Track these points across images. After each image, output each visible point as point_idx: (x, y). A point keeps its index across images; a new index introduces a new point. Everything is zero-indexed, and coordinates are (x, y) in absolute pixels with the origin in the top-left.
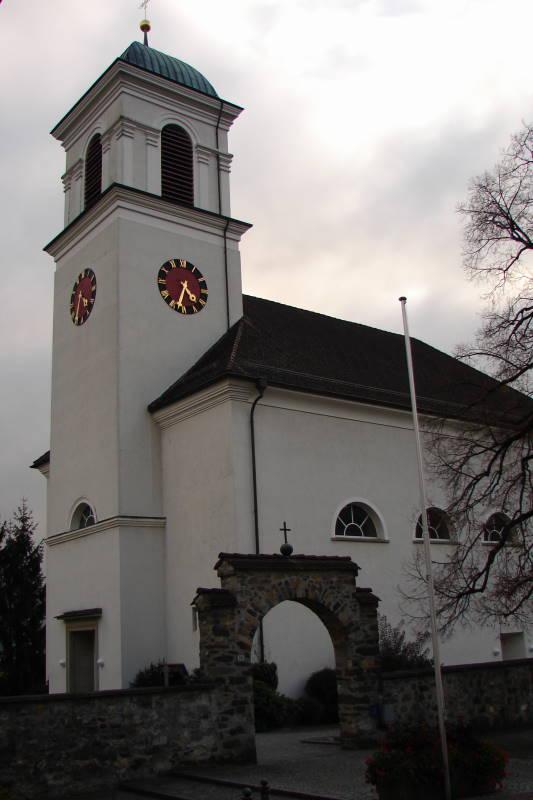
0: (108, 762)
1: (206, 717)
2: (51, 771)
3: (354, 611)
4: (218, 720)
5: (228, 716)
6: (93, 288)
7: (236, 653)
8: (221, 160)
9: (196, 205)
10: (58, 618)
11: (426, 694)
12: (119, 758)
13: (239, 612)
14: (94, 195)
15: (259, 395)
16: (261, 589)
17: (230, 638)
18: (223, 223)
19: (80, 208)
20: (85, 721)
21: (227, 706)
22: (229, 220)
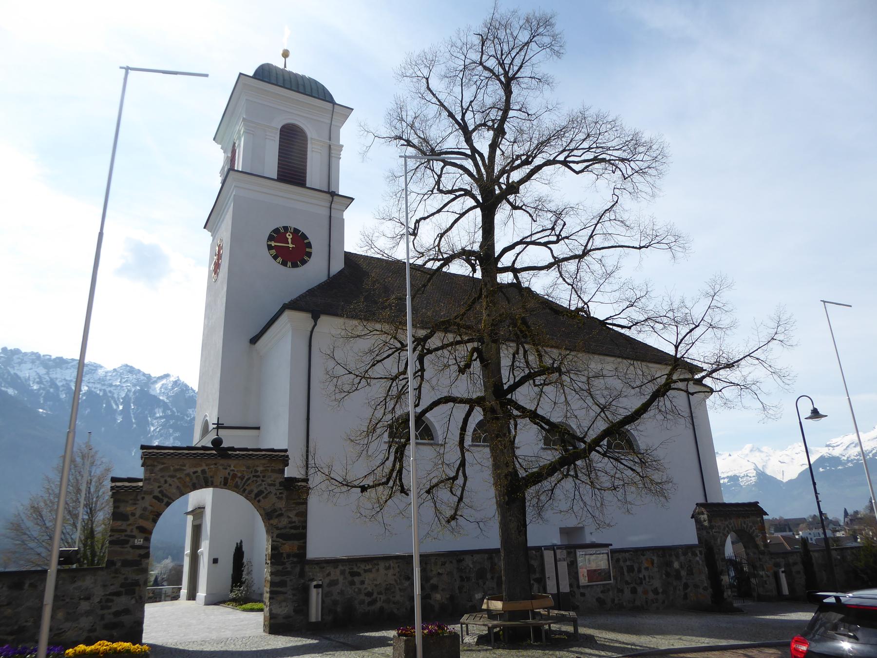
1: (87, 598)
4: (100, 602)
5: (114, 598)
13: (143, 498)
16: (172, 477)
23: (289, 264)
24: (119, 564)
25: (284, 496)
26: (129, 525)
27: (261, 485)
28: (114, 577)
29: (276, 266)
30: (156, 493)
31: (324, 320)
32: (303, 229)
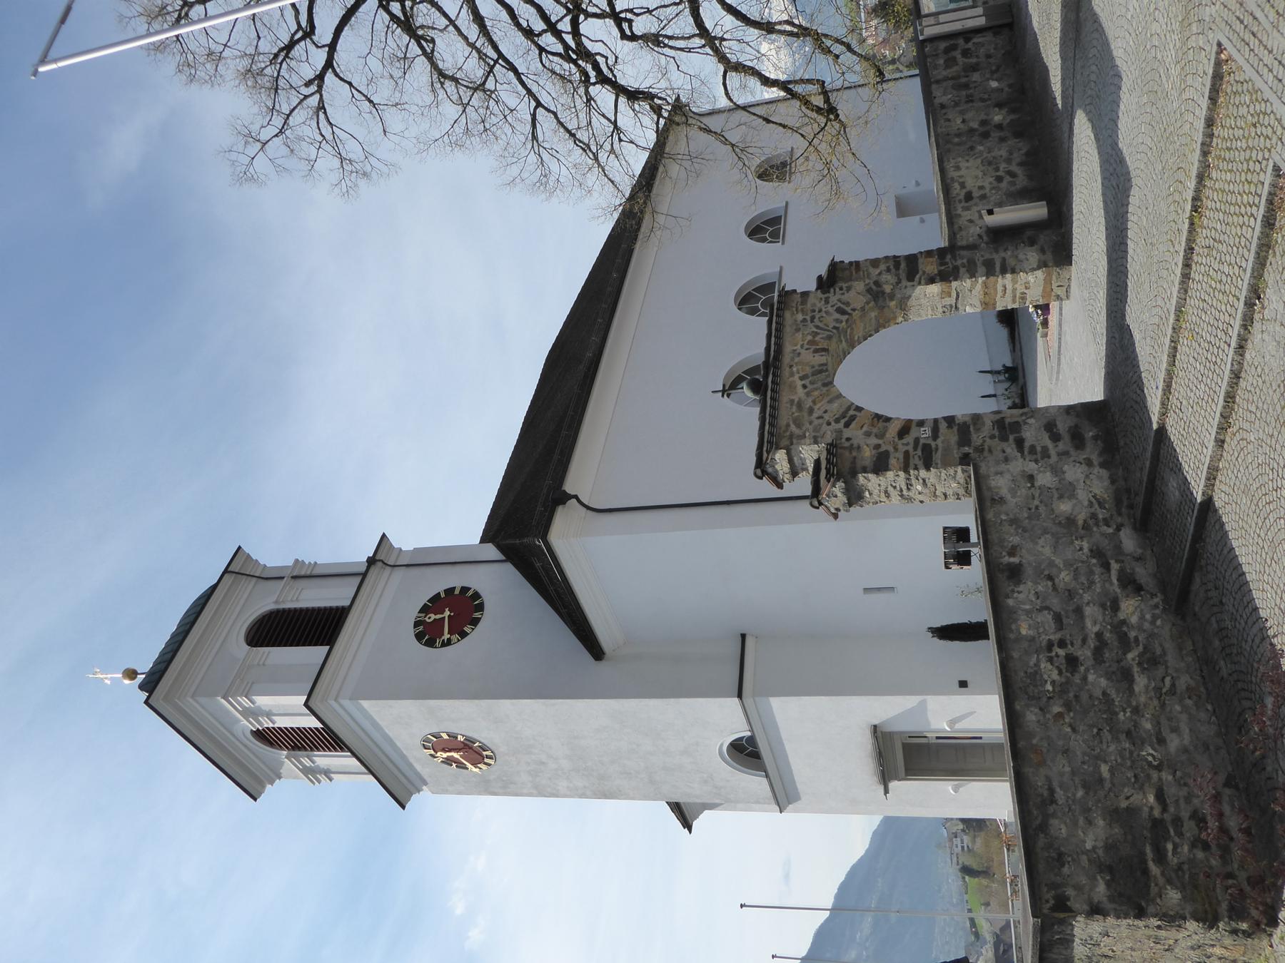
0: (1132, 634)
1: (1031, 478)
2: (1161, 741)
3: (849, 289)
4: (1036, 461)
5: (1027, 444)
6: (445, 736)
7: (917, 440)
8: (303, 574)
9: (347, 603)
10: (886, 792)
11: (976, 194)
12: (1121, 616)
13: (848, 439)
14: (328, 739)
15: (574, 500)
16: (811, 411)
17: (891, 449)
18: (374, 571)
19: (343, 761)
20: (1055, 675)
21: (1010, 449)
22: (371, 561)
23: (477, 615)
24: (966, 449)
25: (844, 285)
26: (896, 449)
27: (827, 312)
28: (990, 451)
29: (477, 635)
30: (841, 425)
31: (569, 487)
32: (424, 599)
